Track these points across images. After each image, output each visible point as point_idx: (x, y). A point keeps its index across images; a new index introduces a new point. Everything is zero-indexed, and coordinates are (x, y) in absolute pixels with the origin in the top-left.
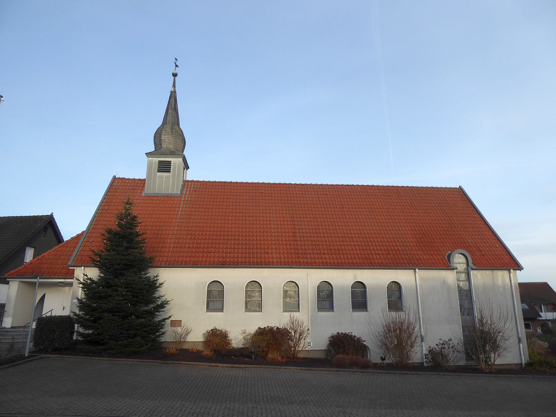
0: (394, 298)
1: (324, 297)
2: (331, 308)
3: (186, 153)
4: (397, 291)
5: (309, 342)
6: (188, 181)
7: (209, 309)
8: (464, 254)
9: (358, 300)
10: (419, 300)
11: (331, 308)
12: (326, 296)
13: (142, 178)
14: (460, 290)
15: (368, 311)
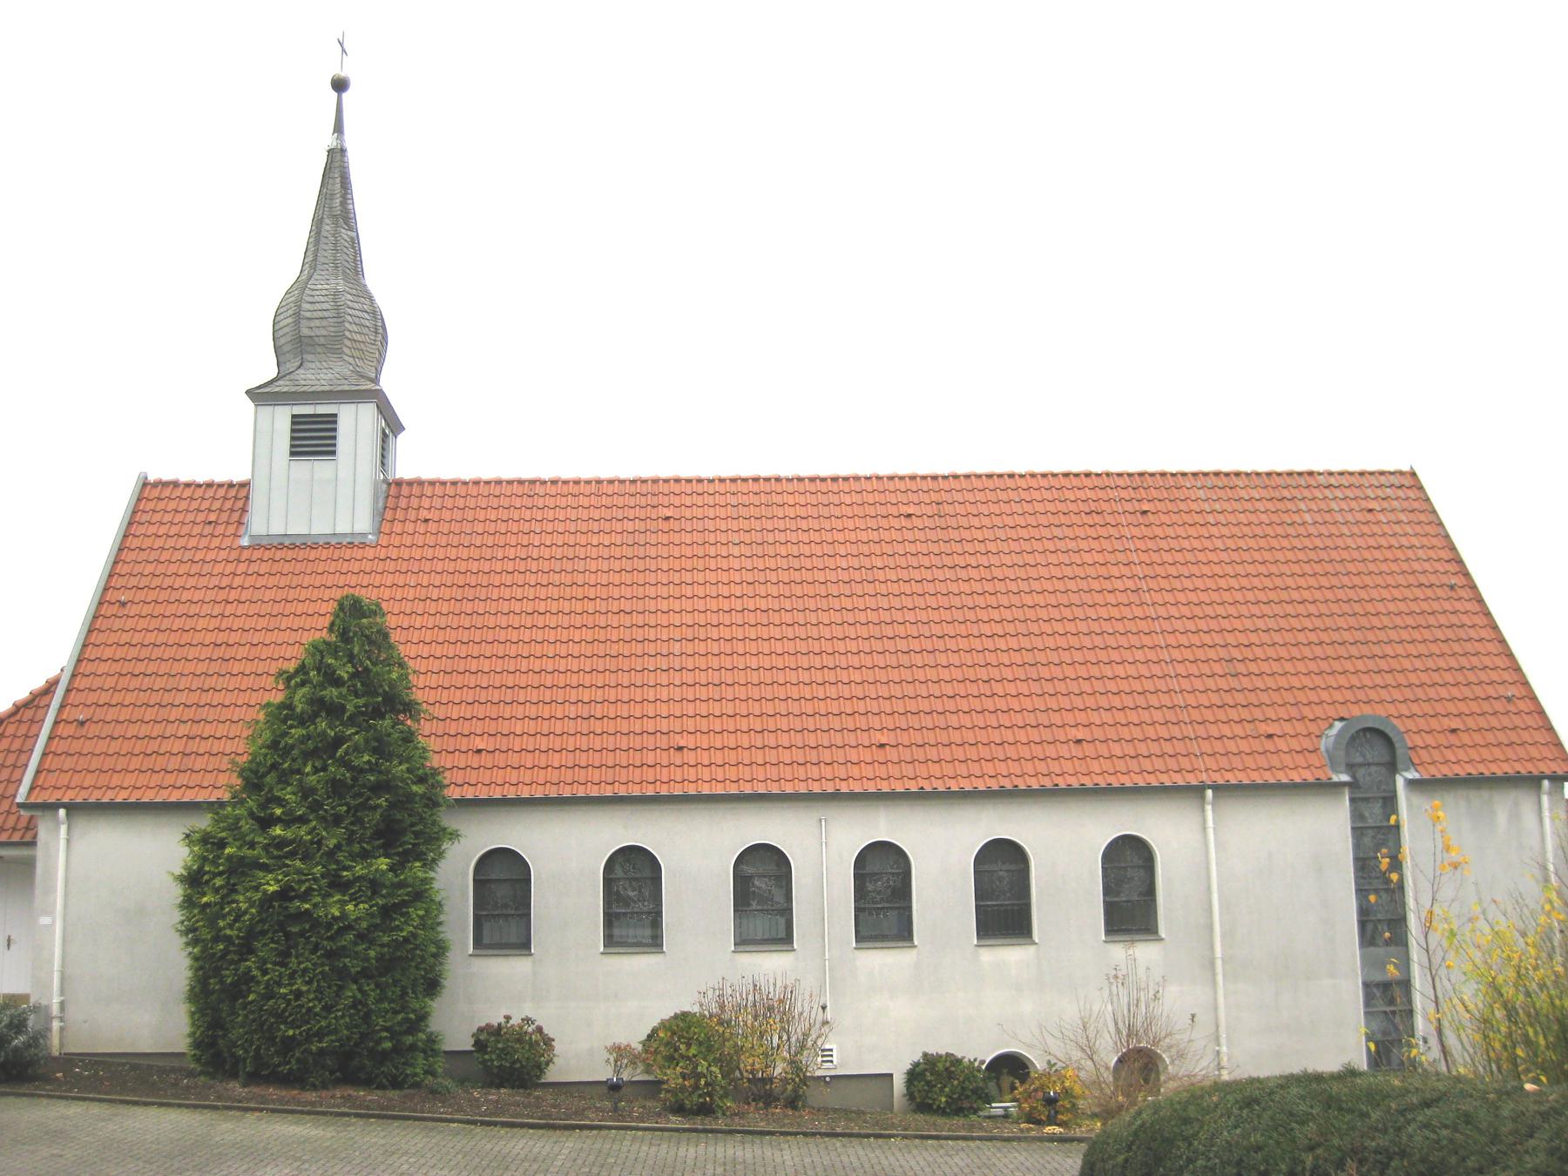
0: (1129, 894)
1: (878, 897)
2: (902, 933)
3: (391, 382)
4: (1139, 867)
5: (827, 1061)
6: (399, 483)
7: (613, 941)
8: (1382, 728)
9: (1001, 905)
10: (1215, 897)
11: (902, 933)
12: (889, 891)
13: (237, 479)
14: (1363, 860)
15: (1034, 943)
